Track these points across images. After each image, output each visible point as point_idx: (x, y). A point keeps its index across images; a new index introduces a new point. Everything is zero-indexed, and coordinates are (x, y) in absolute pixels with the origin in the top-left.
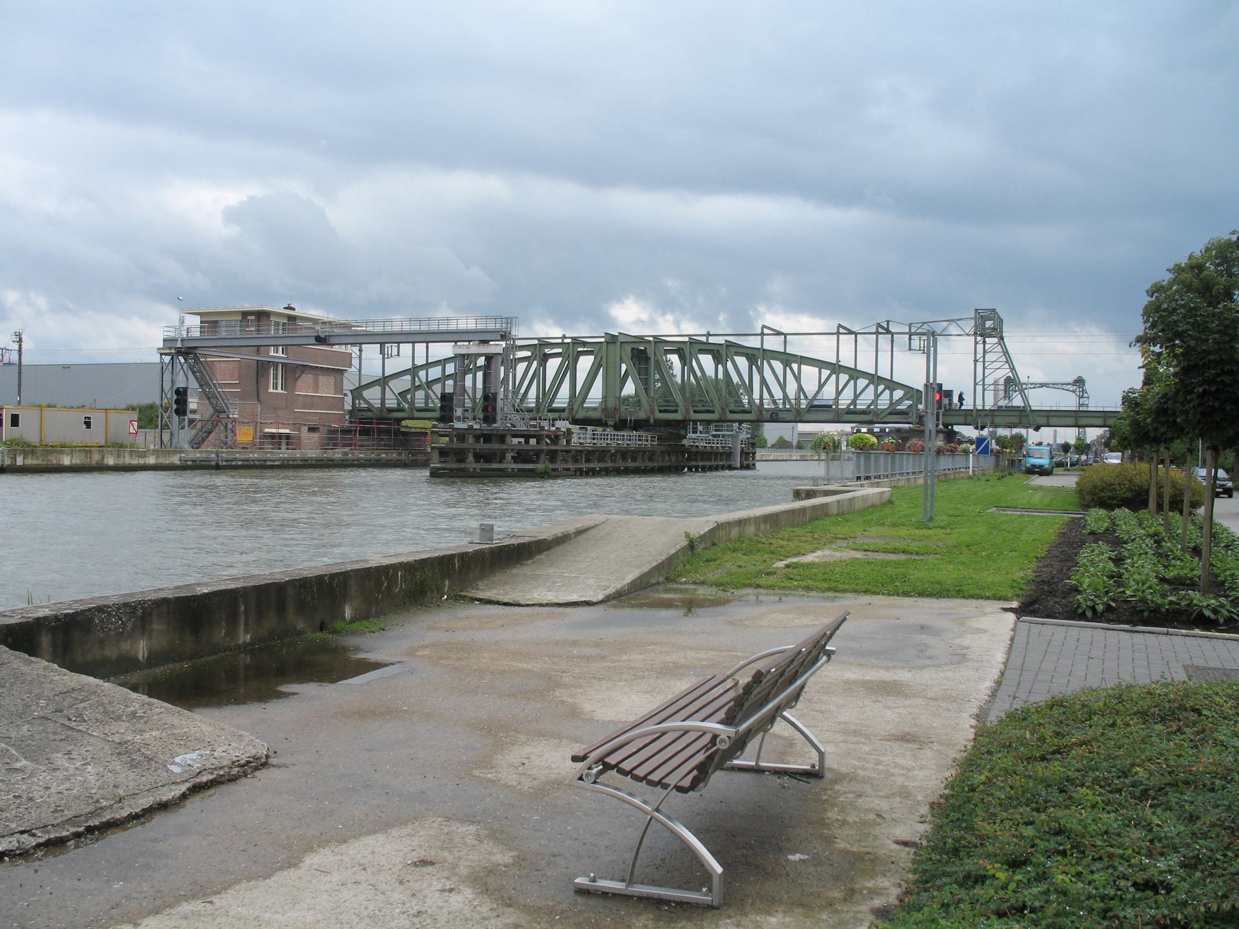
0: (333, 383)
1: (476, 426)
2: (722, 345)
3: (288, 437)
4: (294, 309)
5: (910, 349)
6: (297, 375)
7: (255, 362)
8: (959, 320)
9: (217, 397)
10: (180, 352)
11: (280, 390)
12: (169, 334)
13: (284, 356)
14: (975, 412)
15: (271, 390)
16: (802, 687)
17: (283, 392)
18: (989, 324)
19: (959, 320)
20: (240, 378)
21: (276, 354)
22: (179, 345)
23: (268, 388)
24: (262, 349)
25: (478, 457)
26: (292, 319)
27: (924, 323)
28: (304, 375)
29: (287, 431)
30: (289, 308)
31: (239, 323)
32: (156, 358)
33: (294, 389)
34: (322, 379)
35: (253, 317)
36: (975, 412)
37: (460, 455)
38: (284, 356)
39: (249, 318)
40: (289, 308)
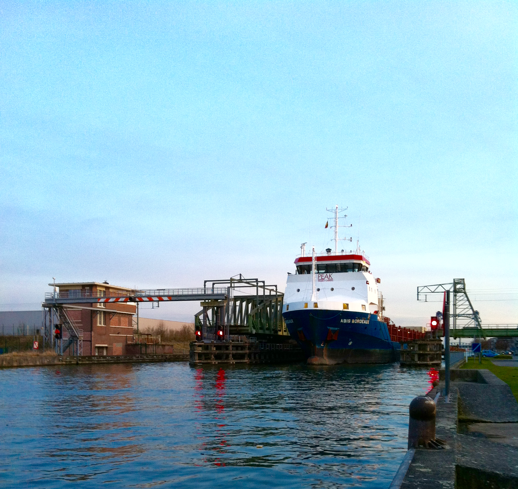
0: (127, 321)
1: (215, 342)
2: (41, 311)
3: (107, 347)
4: (108, 284)
5: (418, 300)
6: (111, 317)
7: (90, 311)
8: (443, 284)
9: (72, 329)
10: (54, 306)
11: (103, 325)
12: (48, 297)
13: (104, 307)
14: (454, 330)
15: (99, 325)
16: (203, 445)
17: (103, 325)
18: (458, 286)
19: (443, 284)
20: (82, 319)
21: (100, 307)
22: (54, 302)
23: (96, 323)
24: (94, 304)
25: (235, 357)
26: (108, 288)
27: (425, 286)
28: (114, 317)
29: (106, 345)
30: (106, 283)
31: (80, 291)
32: (41, 309)
33: (109, 324)
34: (122, 319)
35: (88, 288)
36: (454, 330)
37: (207, 356)
38: (104, 307)
39: (86, 288)
40: (106, 283)
